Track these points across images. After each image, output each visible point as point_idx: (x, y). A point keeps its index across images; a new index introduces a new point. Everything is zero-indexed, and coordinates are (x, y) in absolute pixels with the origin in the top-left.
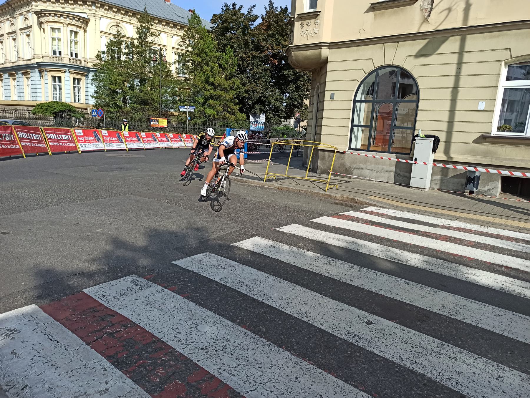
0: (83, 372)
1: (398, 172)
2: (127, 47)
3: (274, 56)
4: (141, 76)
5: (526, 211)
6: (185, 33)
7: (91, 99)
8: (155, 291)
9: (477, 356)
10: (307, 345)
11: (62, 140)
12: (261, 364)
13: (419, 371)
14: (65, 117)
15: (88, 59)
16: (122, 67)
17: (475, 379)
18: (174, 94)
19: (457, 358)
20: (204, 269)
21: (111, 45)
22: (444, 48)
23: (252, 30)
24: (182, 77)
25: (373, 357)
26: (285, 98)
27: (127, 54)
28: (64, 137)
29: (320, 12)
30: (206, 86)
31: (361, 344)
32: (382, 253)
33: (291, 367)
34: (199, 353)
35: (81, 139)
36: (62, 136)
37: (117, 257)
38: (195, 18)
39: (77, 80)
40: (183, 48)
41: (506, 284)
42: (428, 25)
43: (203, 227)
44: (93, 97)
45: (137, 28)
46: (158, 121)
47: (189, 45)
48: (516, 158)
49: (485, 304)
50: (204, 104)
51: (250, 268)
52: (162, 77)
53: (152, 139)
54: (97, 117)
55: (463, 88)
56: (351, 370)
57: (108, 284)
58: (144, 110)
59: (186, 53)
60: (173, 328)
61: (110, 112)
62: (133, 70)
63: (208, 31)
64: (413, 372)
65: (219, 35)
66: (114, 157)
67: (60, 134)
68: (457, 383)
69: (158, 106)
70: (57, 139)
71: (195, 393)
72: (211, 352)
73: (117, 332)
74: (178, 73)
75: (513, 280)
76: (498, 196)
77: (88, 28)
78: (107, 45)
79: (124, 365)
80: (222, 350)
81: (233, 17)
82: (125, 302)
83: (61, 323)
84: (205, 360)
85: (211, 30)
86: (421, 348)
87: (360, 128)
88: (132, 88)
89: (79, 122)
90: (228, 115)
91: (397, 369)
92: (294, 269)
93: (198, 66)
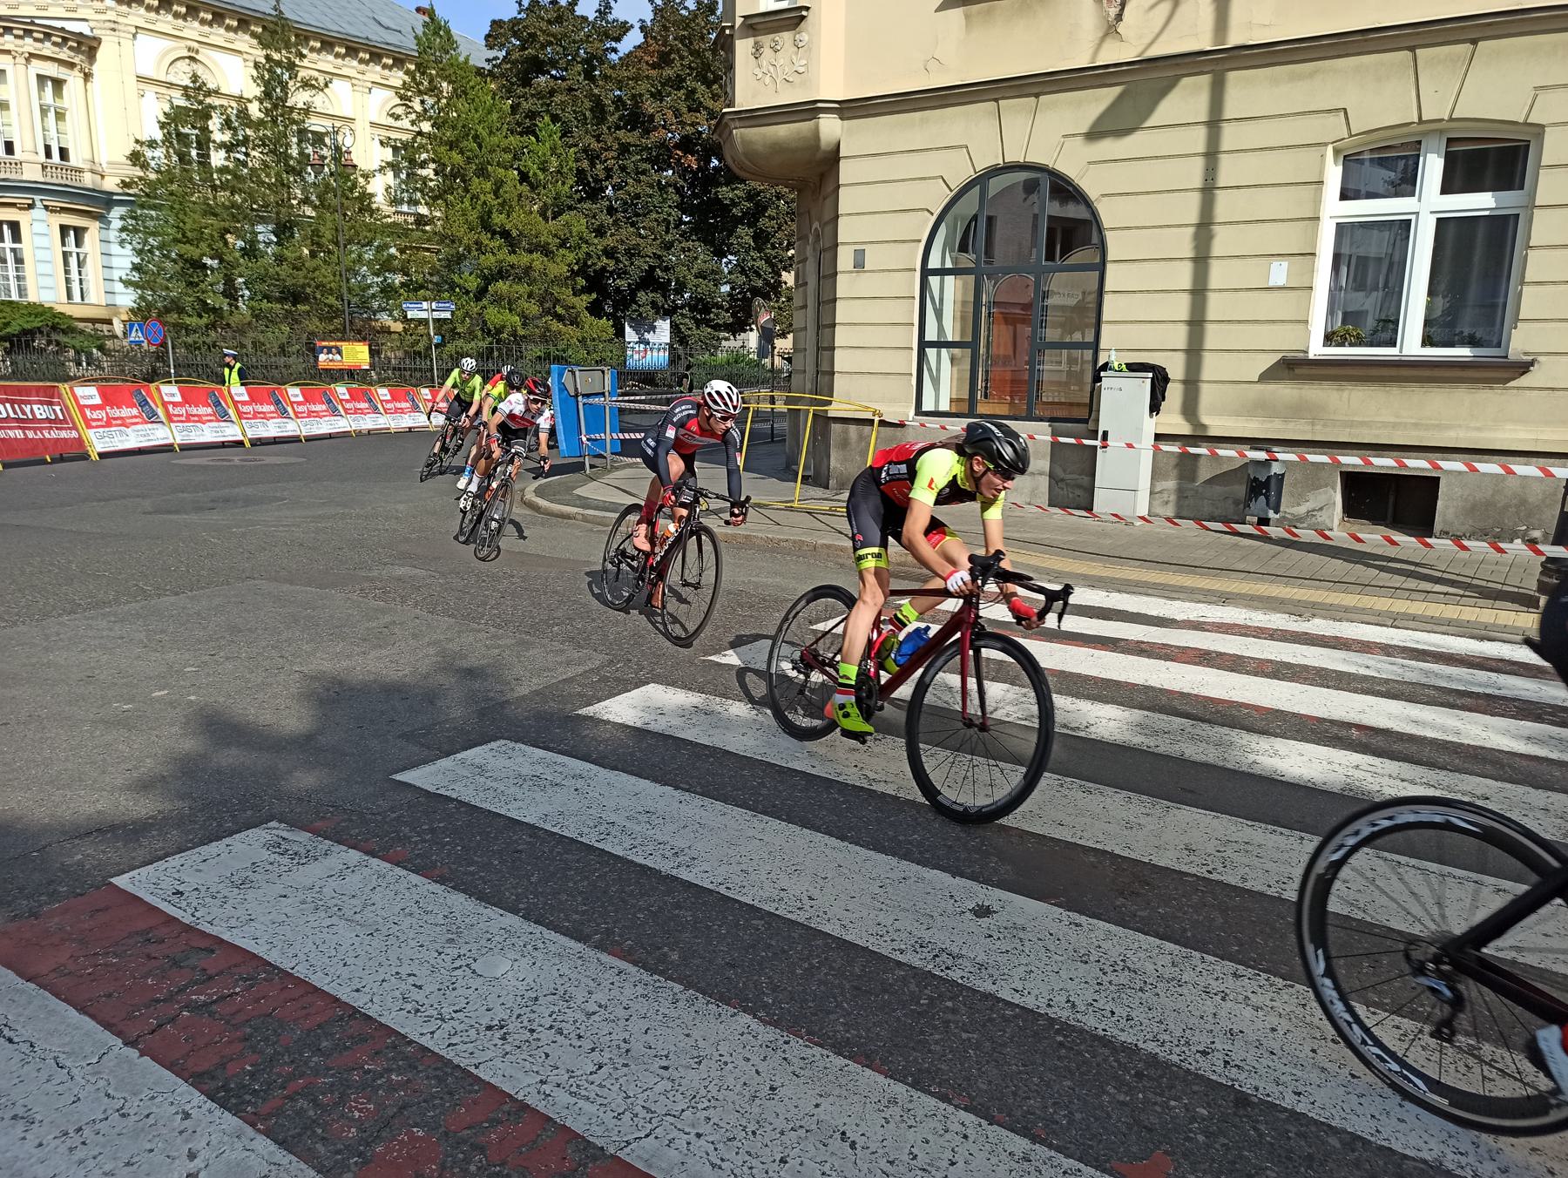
0: (117, 1130)
1: (1059, 473)
2: (227, 124)
3: (687, 144)
4: (278, 213)
5: (1412, 568)
6: (407, 78)
7: (124, 290)
8: (341, 866)
9: (1280, 982)
10: (804, 991)
11: (35, 420)
12: (667, 1057)
13: (1123, 1037)
14: (42, 351)
15: (104, 165)
16: (214, 188)
17: (1276, 1046)
18: (386, 266)
19: (1227, 991)
20: (491, 791)
21: (173, 120)
22: (1169, 109)
23: (613, 67)
24: (408, 214)
25: (992, 1010)
26: (726, 270)
27: (229, 148)
28: (41, 412)
29: (807, 9)
30: (485, 238)
31: (959, 973)
32: (1016, 708)
33: (755, 1059)
34: (479, 1042)
35: (96, 414)
36: (32, 410)
37: (219, 772)
38: (436, 33)
39: (72, 233)
40: (405, 123)
41: (1358, 774)
42: (1118, 43)
43: (489, 666)
44: (127, 283)
45: (257, 65)
46: (339, 352)
47: (423, 116)
48: (1377, 419)
49: (1303, 834)
50: (481, 293)
51: (633, 779)
52: (345, 215)
53: (324, 407)
54: (145, 345)
55: (1225, 223)
56: (930, 1051)
57: (192, 857)
58: (293, 319)
59: (414, 140)
60: (397, 973)
61: (186, 329)
62: (251, 196)
63: (479, 72)
64: (1105, 1042)
65: (512, 84)
66: (205, 468)
67: (29, 402)
68: (1227, 1063)
69: (338, 304)
70: (18, 420)
71: (467, 1161)
72: (516, 1036)
73: (222, 998)
74: (395, 201)
75: (1376, 761)
76: (1335, 528)
77: (96, 68)
78: (163, 119)
79: (248, 1097)
80: (551, 1027)
81: (555, 29)
82: (248, 906)
83: (41, 986)
84: (498, 1062)
85: (488, 67)
86: (1126, 973)
87: (944, 351)
88: (251, 251)
89: (88, 364)
90: (556, 326)
91: (1060, 1038)
92: (764, 771)
93: (453, 178)
